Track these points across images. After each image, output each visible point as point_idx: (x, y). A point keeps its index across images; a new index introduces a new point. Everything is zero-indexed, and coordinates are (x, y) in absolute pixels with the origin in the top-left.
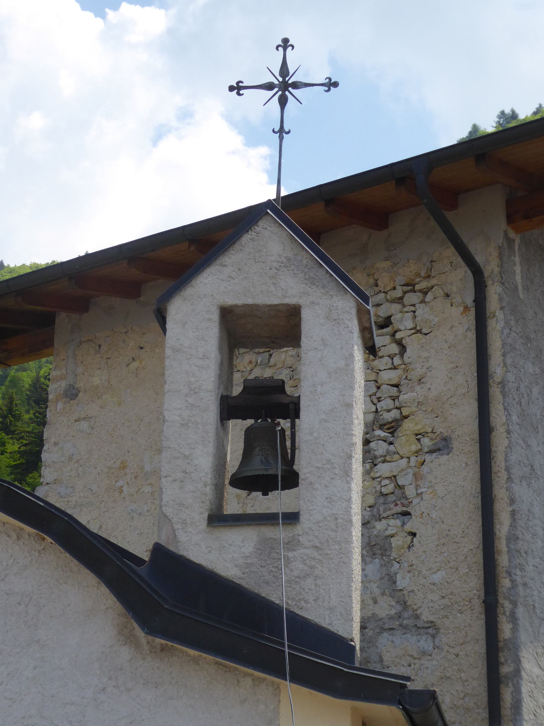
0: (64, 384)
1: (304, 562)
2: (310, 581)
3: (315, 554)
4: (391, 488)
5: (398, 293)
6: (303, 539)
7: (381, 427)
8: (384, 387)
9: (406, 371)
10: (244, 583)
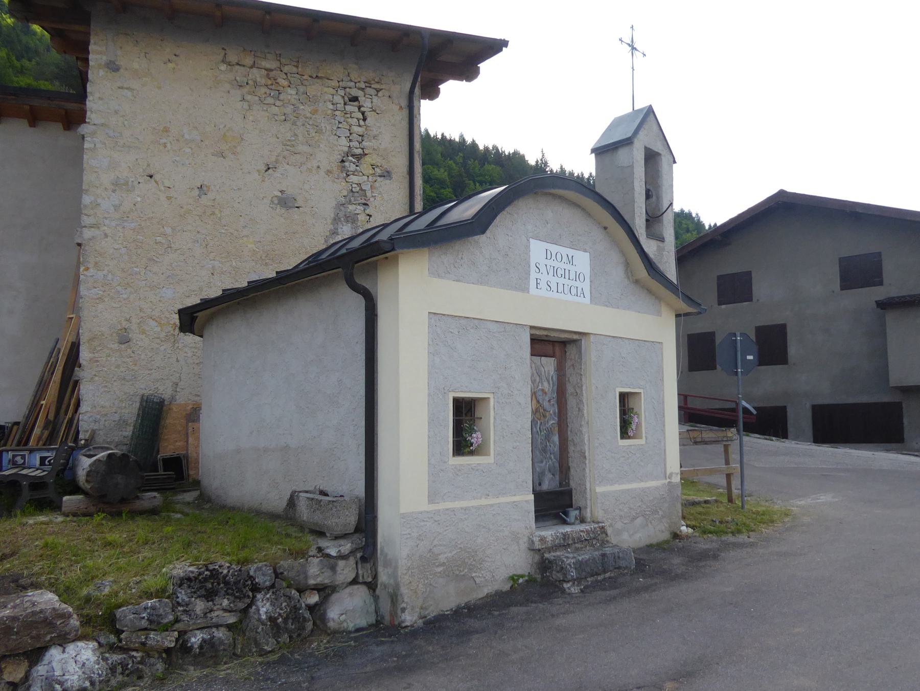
4: (358, 189)
7: (352, 156)
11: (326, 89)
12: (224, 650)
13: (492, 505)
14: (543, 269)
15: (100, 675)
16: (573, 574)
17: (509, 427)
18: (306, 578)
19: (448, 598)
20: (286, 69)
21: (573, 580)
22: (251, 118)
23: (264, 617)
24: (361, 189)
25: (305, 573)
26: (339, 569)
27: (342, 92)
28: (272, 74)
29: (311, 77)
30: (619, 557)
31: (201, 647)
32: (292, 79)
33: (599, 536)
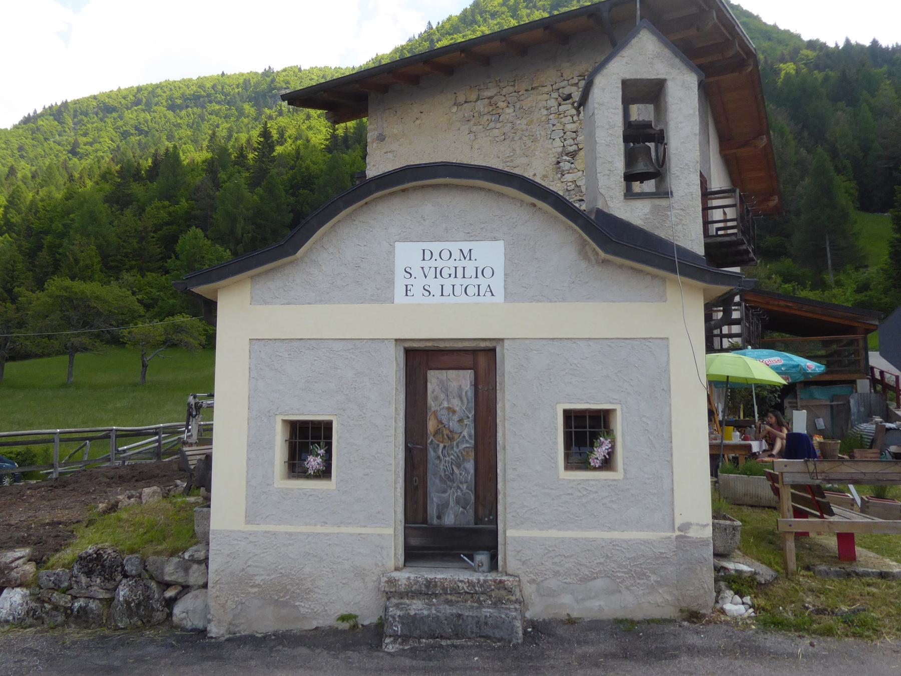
0: (376, 133)
1: (676, 217)
2: (680, 226)
3: (682, 213)
4: (573, 186)
5: (576, 80)
6: (675, 205)
7: (567, 155)
8: (568, 133)
9: (580, 124)
10: (645, 228)
11: (540, 97)
12: (93, 618)
13: (327, 535)
14: (417, 272)
15: (19, 614)
16: (398, 628)
17: (372, 448)
18: (162, 573)
19: (266, 622)
20: (504, 91)
21: (395, 636)
22: (477, 147)
23: (121, 599)
24: (577, 186)
25: (162, 570)
26: (191, 571)
27: (555, 95)
28: (493, 101)
29: (527, 90)
30: (486, 623)
31: (78, 611)
32: (509, 99)
33: (502, 594)
